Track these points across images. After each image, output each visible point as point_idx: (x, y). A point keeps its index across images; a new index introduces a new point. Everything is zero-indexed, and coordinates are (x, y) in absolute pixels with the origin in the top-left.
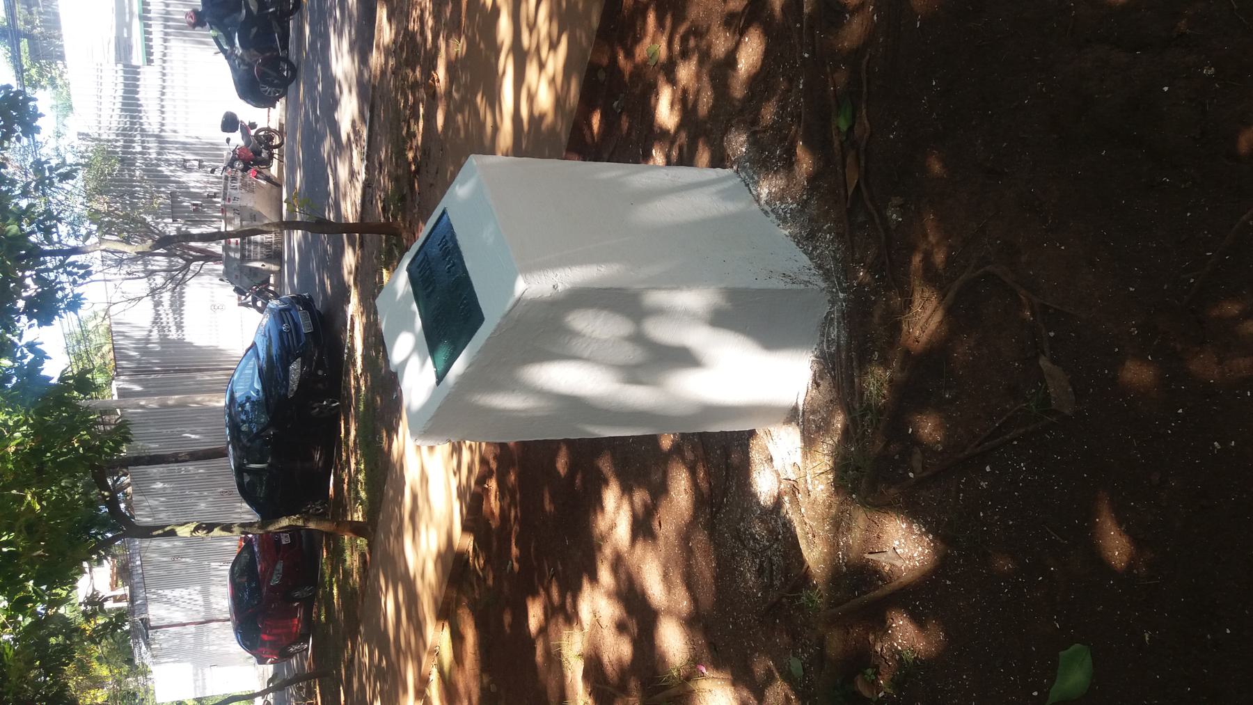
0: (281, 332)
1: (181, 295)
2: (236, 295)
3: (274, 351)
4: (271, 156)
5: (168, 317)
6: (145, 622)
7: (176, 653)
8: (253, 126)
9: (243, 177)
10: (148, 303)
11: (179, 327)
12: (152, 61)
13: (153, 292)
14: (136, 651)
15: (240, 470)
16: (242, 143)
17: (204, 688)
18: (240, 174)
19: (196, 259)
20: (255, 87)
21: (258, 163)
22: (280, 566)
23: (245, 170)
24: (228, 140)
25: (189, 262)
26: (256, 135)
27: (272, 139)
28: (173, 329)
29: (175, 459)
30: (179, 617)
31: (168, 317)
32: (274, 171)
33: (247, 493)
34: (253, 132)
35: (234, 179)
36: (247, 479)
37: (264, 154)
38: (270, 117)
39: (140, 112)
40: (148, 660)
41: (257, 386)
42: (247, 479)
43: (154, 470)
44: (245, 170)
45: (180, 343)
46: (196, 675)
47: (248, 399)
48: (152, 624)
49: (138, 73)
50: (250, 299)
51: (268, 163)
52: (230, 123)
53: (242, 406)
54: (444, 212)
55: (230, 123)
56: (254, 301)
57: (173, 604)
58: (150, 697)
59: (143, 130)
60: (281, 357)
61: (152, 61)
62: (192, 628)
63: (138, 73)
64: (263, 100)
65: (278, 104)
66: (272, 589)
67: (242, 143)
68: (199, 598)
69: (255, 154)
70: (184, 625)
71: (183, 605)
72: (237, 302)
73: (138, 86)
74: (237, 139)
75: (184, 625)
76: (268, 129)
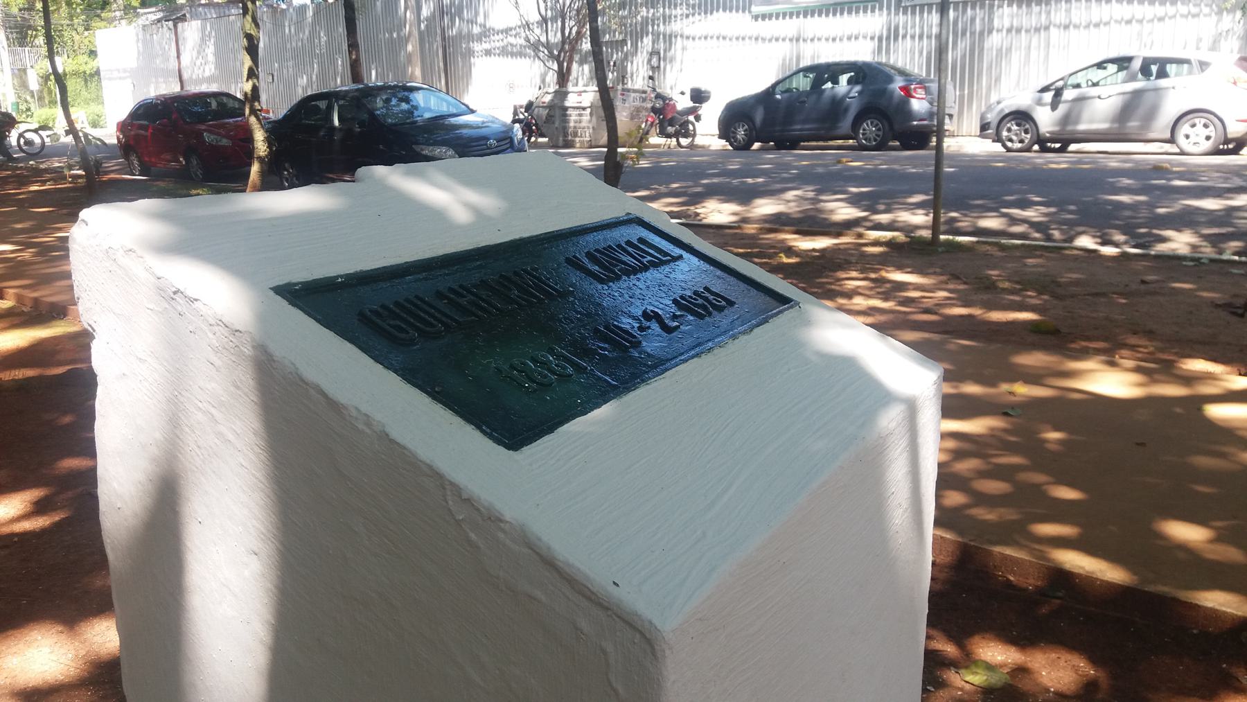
0: (486, 138)
1: (521, 54)
2: (525, 103)
3: (464, 131)
4: (669, 136)
5: (496, 42)
6: (183, 19)
7: (148, 52)
8: (698, 118)
9: (646, 109)
10: (514, 21)
11: (488, 53)
12: (756, 20)
13: (527, 26)
14: (153, 9)
15: (330, 97)
16: (679, 107)
17: (110, 79)
18: (649, 105)
19: (560, 65)
20: (737, 118)
21: (661, 123)
22: (225, 142)
23: (654, 110)
24: (683, 93)
25: (557, 58)
26: (688, 122)
27: (686, 136)
28: (486, 46)
29: (353, 45)
30: (186, 59)
31: (496, 42)
32: (655, 140)
33: (306, 107)
34: (691, 118)
35: (644, 100)
36: (323, 104)
37: (670, 129)
38: (707, 133)
39: (706, 13)
40: (141, 21)
41: (427, 115)
42: (323, 104)
43: (342, 29)
44: (654, 110)
45: (470, 53)
46: (125, 71)
47: (416, 108)
48: (180, 25)
49: (744, 11)
50: (521, 117)
51: (663, 133)
52: (699, 96)
53: (407, 100)
54: (784, 300)
55: (699, 96)
56: (519, 121)
57: (199, 53)
58: (104, 23)
59: (687, 16)
60: (460, 137)
61: (756, 20)
62: (173, 64)
63: (744, 11)
64: (727, 128)
65: (723, 142)
66: (199, 135)
67: (679, 107)
68: (207, 74)
69: (670, 120)
70: (178, 57)
71: (198, 63)
72: (518, 103)
73: (731, 11)
74: (683, 103)
75: (178, 57)
76: (694, 136)
